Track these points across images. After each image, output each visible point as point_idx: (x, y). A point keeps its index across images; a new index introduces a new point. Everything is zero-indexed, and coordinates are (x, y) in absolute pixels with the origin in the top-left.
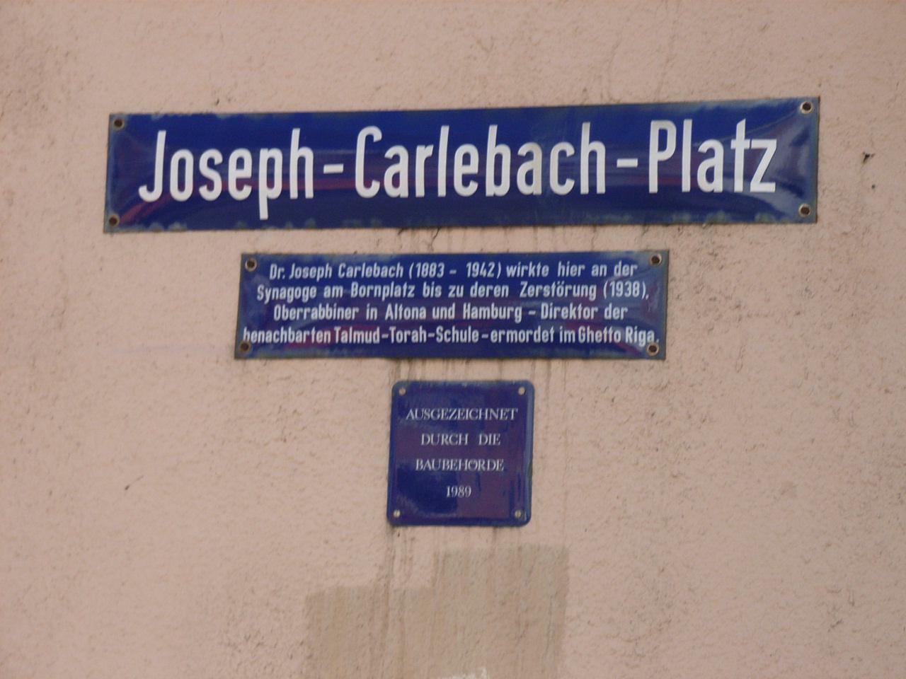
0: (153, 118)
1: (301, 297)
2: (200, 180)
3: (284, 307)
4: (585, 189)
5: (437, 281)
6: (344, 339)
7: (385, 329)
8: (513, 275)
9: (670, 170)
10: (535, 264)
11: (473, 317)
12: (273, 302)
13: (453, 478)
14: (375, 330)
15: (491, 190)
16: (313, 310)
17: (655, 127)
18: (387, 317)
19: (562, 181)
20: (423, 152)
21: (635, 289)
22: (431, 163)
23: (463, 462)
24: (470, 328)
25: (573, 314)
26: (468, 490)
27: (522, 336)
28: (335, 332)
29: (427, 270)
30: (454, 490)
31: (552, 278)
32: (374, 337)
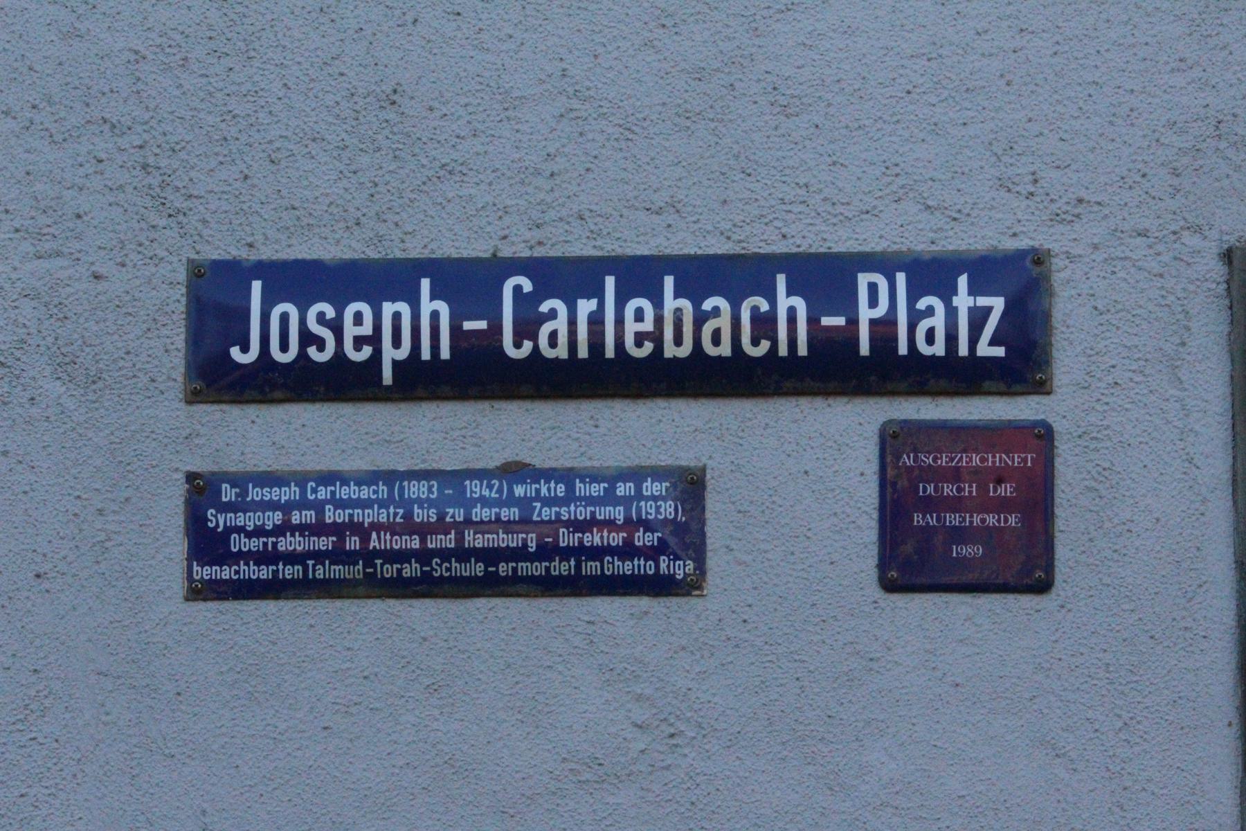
0: (245, 264)
1: (264, 523)
2: (308, 338)
3: (242, 535)
4: (783, 351)
5: (431, 503)
6: (320, 574)
7: (369, 563)
8: (522, 495)
9: (884, 329)
10: (547, 482)
11: (477, 545)
12: (229, 530)
13: (960, 535)
14: (357, 563)
15: (670, 351)
16: (280, 539)
17: (863, 279)
18: (371, 548)
19: (755, 342)
20: (586, 307)
21: (668, 509)
22: (596, 320)
23: (971, 516)
24: (473, 560)
25: (597, 540)
26: (978, 549)
27: (537, 569)
28: (308, 565)
29: (417, 490)
30: (962, 549)
31: (570, 498)
32: (357, 570)
